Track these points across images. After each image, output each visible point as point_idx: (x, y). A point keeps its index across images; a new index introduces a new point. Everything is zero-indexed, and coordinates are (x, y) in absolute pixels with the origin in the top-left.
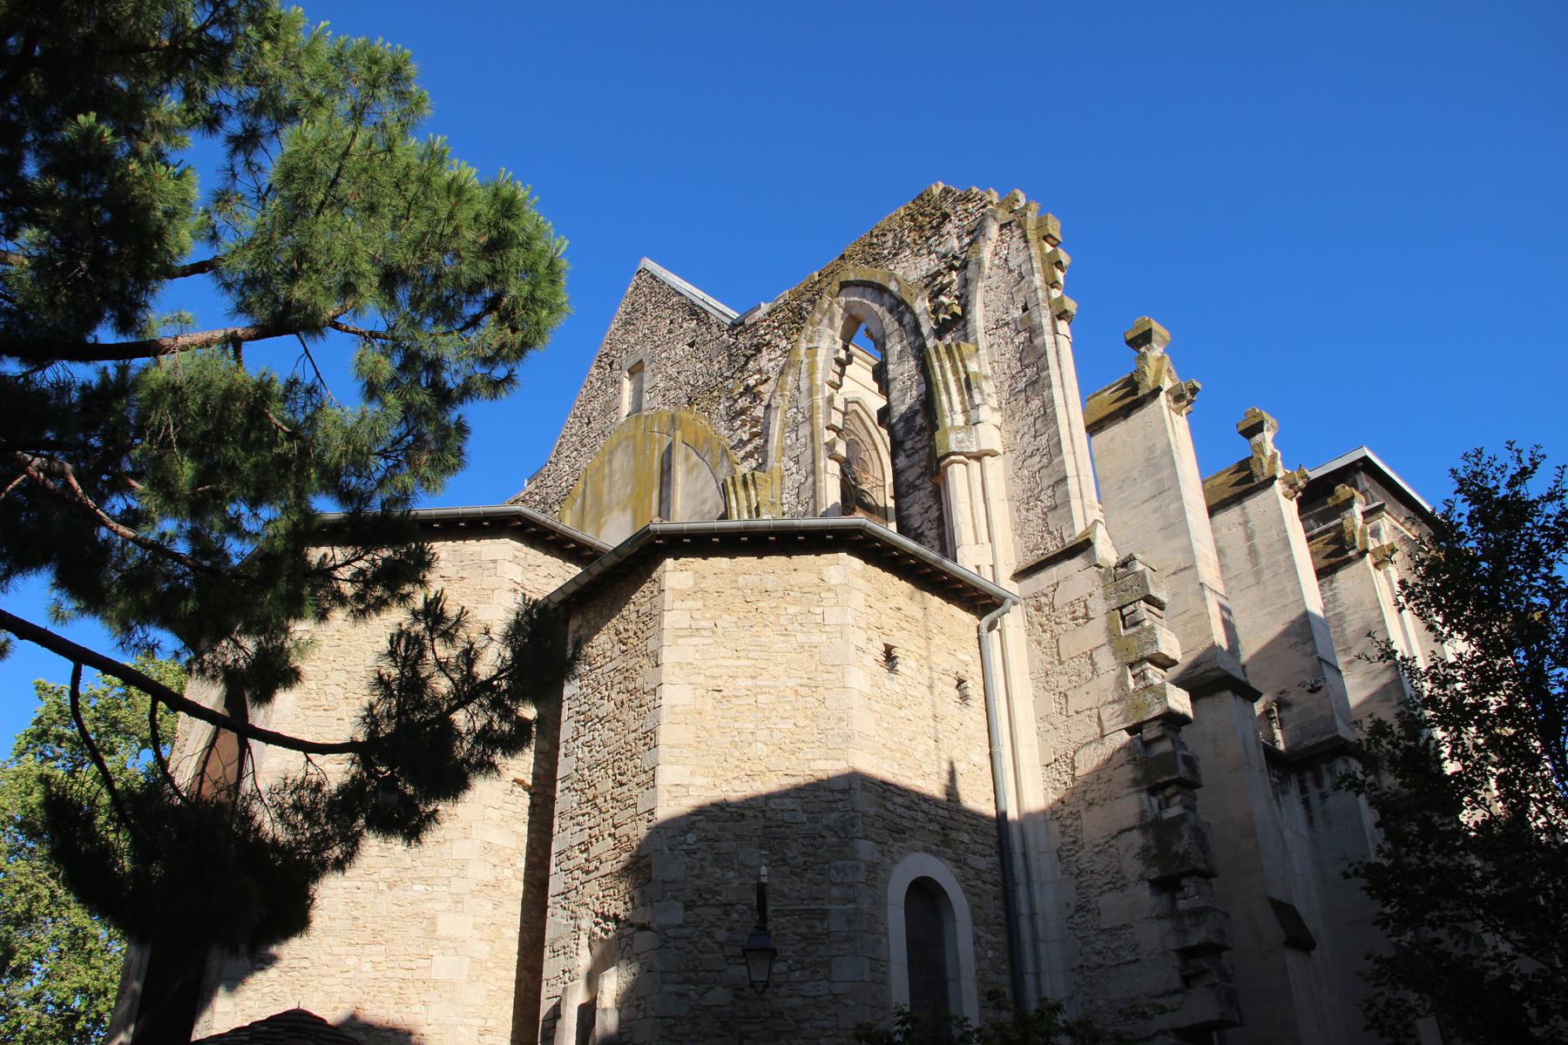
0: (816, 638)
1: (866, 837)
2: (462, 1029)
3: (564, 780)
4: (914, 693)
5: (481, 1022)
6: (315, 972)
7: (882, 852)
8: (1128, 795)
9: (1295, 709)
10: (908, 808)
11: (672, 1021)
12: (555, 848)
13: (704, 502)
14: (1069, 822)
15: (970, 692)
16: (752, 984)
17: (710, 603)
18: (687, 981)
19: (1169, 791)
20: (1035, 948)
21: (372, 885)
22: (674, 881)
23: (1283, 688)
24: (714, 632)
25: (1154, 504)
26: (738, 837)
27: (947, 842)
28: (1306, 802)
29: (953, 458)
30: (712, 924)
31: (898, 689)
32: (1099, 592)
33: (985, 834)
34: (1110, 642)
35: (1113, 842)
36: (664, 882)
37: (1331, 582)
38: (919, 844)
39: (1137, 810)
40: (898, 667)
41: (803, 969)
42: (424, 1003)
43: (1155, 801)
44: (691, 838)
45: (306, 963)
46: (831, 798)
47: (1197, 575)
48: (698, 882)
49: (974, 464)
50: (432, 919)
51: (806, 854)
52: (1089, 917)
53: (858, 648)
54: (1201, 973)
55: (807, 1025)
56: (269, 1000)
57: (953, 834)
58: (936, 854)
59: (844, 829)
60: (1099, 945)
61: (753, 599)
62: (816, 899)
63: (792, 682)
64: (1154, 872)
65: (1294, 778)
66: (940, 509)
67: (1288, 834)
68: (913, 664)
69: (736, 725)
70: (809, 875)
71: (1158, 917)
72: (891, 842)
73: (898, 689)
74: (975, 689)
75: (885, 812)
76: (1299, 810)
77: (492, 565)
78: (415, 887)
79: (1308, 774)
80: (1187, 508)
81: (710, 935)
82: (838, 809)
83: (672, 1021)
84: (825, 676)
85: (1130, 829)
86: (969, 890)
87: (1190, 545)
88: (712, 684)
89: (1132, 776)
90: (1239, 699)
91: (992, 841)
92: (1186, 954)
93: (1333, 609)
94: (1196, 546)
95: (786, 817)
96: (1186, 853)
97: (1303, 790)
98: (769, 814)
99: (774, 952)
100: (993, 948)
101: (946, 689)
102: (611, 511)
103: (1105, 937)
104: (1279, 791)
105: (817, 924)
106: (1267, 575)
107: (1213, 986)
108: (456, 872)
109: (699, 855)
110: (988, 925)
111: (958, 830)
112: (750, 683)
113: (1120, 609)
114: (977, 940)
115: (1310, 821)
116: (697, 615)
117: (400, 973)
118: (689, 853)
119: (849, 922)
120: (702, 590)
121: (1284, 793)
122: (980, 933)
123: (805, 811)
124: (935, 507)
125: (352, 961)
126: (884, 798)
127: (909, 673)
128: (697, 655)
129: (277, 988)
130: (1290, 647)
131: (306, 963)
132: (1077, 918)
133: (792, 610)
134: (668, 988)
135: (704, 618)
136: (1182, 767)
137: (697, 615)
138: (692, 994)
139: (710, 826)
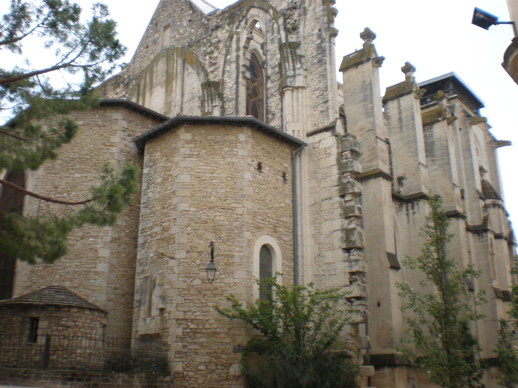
0: (235, 160)
1: (248, 231)
2: (108, 288)
3: (144, 203)
4: (268, 180)
5: (113, 286)
7: (253, 236)
8: (338, 219)
10: (263, 220)
11: (181, 290)
12: (140, 227)
13: (193, 89)
14: (317, 225)
15: (287, 178)
16: (208, 280)
17: (197, 145)
18: (186, 277)
19: (352, 219)
20: (303, 267)
21: (74, 238)
22: (183, 243)
23: (405, 172)
24: (198, 156)
25: (363, 104)
26: (205, 229)
27: (275, 232)
28: (408, 214)
30: (195, 258)
31: (262, 178)
32: (335, 145)
33: (289, 228)
34: (337, 164)
35: (332, 234)
36: (180, 244)
37: (431, 128)
40: (263, 170)
41: (225, 274)
43: (347, 221)
44: (189, 229)
47: (375, 133)
48: (191, 244)
50: (96, 251)
51: (227, 236)
52: (321, 258)
53: (249, 164)
54: (355, 280)
55: (225, 292)
57: (277, 229)
58: (271, 236)
59: (240, 228)
60: (324, 268)
61: (212, 144)
62: (230, 251)
63: (225, 176)
64: (344, 246)
65: (405, 205)
66: (282, 105)
67: (399, 226)
68: (267, 169)
69: (205, 190)
70: (228, 243)
71: (344, 261)
72: (256, 232)
73: (262, 178)
74: (289, 177)
75: (254, 222)
76: (405, 217)
77: (116, 121)
79: (410, 205)
80: (375, 106)
81: (194, 262)
82: (238, 221)
83: (181, 290)
84: (237, 174)
85: (337, 230)
86: (282, 248)
88: (197, 175)
89: (340, 212)
90: (385, 180)
91: (291, 231)
92: (352, 274)
93: (430, 139)
95: (221, 223)
96: (355, 241)
97: (407, 210)
99: (216, 270)
100: (289, 267)
101: (279, 177)
102: (156, 86)
103: (326, 266)
104: (399, 209)
105: (230, 259)
106: (404, 129)
107: (358, 285)
108: (104, 234)
109: (192, 235)
110: (288, 259)
111: (280, 227)
112: (210, 175)
114: (283, 264)
115: (408, 221)
116: (193, 150)
117: (86, 269)
118: (188, 234)
119: (241, 259)
120: (194, 140)
121: (400, 211)
122: (284, 262)
123: (228, 221)
124: (280, 104)
125: (68, 265)
126: (255, 217)
127: (265, 172)
128: (193, 164)
132: (317, 259)
133: (226, 149)
135: (195, 151)
137: (193, 150)
138: (188, 281)
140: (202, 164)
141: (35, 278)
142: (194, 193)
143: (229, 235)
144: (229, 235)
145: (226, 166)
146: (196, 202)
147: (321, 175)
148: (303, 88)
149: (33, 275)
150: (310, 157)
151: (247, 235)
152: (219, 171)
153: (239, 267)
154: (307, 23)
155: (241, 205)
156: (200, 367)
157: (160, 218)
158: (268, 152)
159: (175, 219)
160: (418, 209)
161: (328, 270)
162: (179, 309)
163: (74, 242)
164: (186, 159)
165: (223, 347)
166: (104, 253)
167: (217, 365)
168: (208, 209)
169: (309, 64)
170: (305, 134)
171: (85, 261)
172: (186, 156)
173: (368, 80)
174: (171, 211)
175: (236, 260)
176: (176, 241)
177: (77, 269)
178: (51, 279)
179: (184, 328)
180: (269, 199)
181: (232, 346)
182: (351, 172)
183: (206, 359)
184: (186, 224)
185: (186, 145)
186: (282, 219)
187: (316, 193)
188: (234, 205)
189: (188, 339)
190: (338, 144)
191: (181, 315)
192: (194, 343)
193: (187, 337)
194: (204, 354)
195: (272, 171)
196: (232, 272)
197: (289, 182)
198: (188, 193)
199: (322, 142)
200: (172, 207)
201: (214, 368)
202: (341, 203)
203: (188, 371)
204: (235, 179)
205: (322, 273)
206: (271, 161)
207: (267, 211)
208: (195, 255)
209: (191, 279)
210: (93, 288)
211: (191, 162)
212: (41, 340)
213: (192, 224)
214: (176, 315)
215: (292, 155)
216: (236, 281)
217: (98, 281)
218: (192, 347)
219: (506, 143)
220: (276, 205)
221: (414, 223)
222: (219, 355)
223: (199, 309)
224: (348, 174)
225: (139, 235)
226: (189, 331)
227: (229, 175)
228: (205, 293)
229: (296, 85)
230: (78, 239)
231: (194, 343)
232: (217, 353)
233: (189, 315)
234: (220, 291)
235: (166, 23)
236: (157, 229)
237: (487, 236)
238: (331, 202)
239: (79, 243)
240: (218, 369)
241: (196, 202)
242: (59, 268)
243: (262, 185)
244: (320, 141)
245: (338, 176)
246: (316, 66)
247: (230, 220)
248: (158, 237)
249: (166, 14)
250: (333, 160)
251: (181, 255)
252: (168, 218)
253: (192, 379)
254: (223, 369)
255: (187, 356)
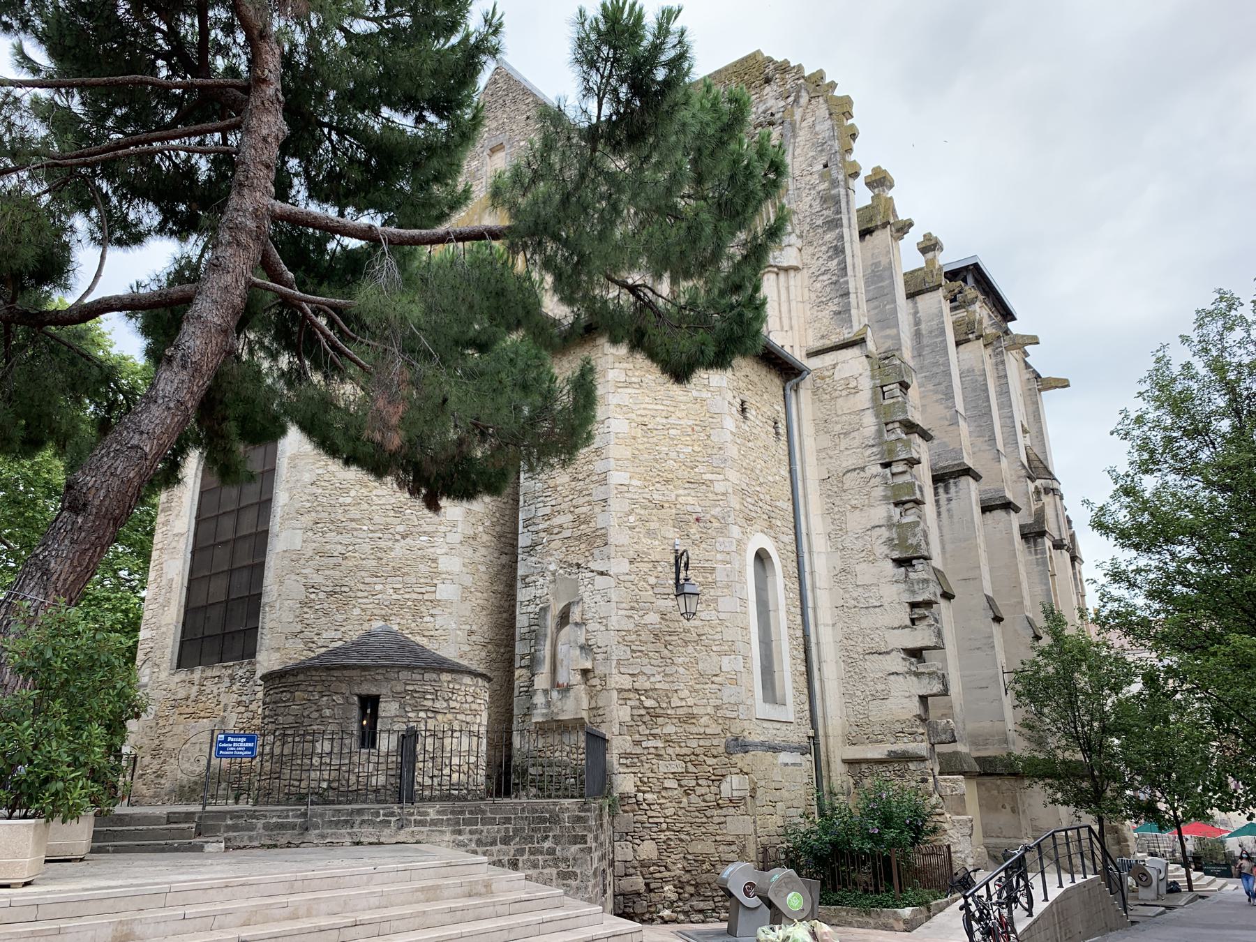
0: (705, 394)
1: (735, 524)
2: (458, 632)
6: (353, 595)
9: (935, 442)
12: (522, 516)
14: (837, 517)
18: (632, 608)
19: (907, 506)
27: (771, 527)
29: (770, 269)
32: (868, 373)
35: (869, 533)
38: (759, 528)
39: (886, 515)
42: (432, 616)
43: (898, 510)
44: (632, 518)
45: (346, 589)
46: (715, 498)
49: (782, 275)
50: (434, 560)
52: (849, 576)
53: (729, 403)
55: (704, 637)
56: (321, 614)
57: (774, 521)
60: (855, 594)
63: (690, 423)
64: (896, 555)
68: (753, 412)
70: (703, 545)
74: (782, 430)
78: (421, 538)
85: (880, 526)
86: (781, 555)
87: (899, 334)
88: (640, 419)
92: (914, 605)
94: (902, 335)
95: (689, 508)
98: (678, 506)
105: (708, 575)
108: (450, 528)
109: (637, 530)
112: (664, 421)
113: (882, 387)
115: (939, 514)
116: (630, 373)
117: (415, 596)
125: (378, 587)
127: (752, 418)
129: (326, 606)
130: (937, 401)
131: (346, 589)
134: (620, 612)
135: (634, 376)
136: (918, 492)
137: (630, 373)
138: (635, 616)
139: (642, 512)
140: (647, 400)
141: (310, 616)
142: (636, 452)
143: (705, 531)
144: (705, 531)
145: (690, 405)
146: (642, 470)
147: (840, 426)
148: (796, 269)
149: (306, 610)
150: (814, 393)
151: (735, 531)
152: (679, 414)
153: (725, 590)
154: (798, 151)
155: (722, 477)
156: (667, 784)
157: (566, 499)
158: (752, 383)
159: (605, 501)
160: (957, 492)
161: (865, 599)
162: (622, 670)
163: (390, 544)
164: (619, 390)
165: (708, 743)
166: (451, 564)
167: (697, 778)
168: (663, 483)
169: (807, 227)
170: (804, 353)
171: (411, 579)
172: (620, 385)
173: (884, 261)
174: (592, 486)
175: (720, 575)
176: (611, 540)
177: (395, 597)
178: (344, 617)
179: (632, 708)
180: (759, 466)
181: (724, 740)
182: (900, 422)
183: (678, 766)
184: (627, 509)
185: (617, 365)
186: (778, 504)
187: (831, 458)
188: (708, 476)
189: (642, 728)
190: (872, 370)
191: (626, 682)
192: (654, 736)
193: (640, 723)
194: (674, 757)
195: (760, 417)
196: (715, 600)
197: (784, 438)
198: (627, 453)
199: (839, 367)
200: (595, 478)
201: (693, 783)
202: (885, 477)
203: (644, 792)
204: (708, 429)
205: (854, 603)
206: (758, 398)
207: (758, 489)
208: (645, 567)
209: (641, 613)
210: (432, 633)
211: (628, 396)
212: (387, 743)
213: (637, 511)
214: (617, 683)
215: (784, 390)
216: (722, 616)
217: (438, 618)
218: (650, 744)
219: (1064, 384)
220: (770, 478)
221: (951, 517)
222: (702, 758)
223: (660, 669)
224: (897, 425)
225: (521, 529)
226: (643, 712)
227: (697, 423)
228: (668, 638)
229: (785, 264)
230: (398, 537)
231: (654, 736)
232: (697, 755)
233: (642, 683)
234: (695, 635)
235: (494, 143)
236: (565, 519)
237: (1044, 544)
238: (862, 474)
239: (397, 545)
240: (700, 785)
241: (642, 470)
242: (360, 594)
243: (749, 441)
244: (834, 366)
245: (876, 427)
246: (821, 231)
247: (703, 503)
248: (567, 533)
249: (494, 125)
250: (864, 398)
251: (619, 566)
252: (587, 498)
253: (653, 807)
254: (709, 786)
255: (642, 761)
